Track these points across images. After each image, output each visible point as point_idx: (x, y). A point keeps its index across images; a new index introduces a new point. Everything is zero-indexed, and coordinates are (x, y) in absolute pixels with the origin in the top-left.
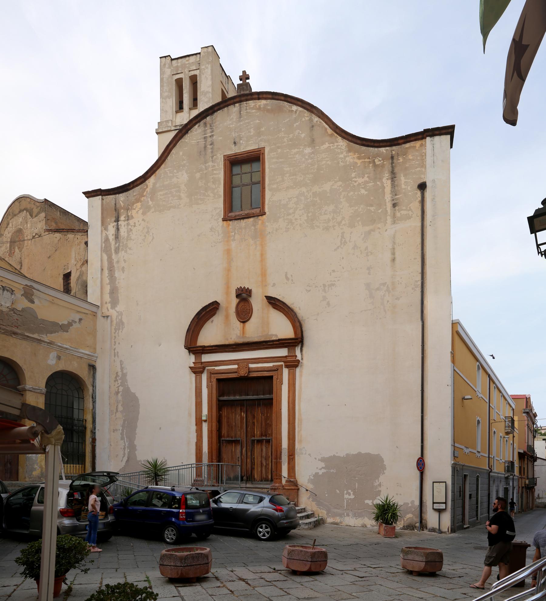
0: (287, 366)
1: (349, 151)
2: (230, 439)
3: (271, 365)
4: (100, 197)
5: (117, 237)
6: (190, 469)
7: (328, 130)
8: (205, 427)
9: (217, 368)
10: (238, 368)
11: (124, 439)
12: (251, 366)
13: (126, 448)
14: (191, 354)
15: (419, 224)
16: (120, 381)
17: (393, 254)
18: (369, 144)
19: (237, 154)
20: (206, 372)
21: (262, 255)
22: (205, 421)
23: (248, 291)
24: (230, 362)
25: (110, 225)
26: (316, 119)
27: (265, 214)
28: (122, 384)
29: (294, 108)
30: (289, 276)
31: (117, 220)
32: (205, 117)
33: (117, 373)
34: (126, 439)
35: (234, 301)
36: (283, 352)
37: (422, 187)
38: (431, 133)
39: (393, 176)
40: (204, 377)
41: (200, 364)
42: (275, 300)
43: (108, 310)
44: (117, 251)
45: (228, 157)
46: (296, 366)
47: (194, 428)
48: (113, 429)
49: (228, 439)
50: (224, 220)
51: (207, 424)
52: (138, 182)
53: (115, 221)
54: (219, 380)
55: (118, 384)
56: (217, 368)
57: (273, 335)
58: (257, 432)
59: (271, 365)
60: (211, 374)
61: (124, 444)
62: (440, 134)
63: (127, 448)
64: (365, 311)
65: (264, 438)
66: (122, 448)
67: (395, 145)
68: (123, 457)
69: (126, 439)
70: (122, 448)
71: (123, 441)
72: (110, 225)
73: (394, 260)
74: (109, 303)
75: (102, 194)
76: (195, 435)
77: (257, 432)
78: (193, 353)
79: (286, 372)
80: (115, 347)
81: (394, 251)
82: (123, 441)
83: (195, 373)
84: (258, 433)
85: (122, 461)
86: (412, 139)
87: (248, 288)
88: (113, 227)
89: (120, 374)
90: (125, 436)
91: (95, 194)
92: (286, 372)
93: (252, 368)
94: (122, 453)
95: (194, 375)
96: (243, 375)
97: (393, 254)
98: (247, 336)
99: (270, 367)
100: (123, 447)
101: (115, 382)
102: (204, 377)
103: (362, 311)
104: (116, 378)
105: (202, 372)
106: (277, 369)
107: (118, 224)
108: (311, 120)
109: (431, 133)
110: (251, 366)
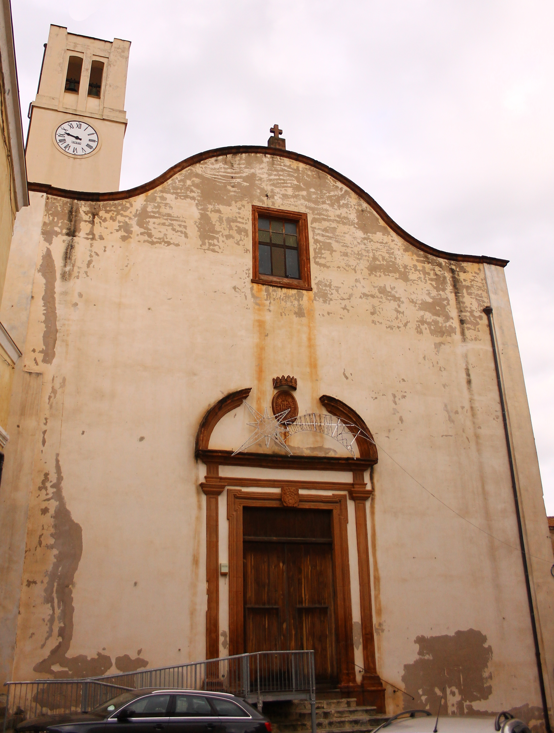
0: (352, 498)
1: (406, 250)
2: (261, 606)
3: (329, 493)
4: (45, 194)
5: (67, 256)
6: (194, 666)
7: (379, 220)
8: (224, 586)
9: (245, 490)
10: (281, 495)
11: (52, 601)
12: (302, 492)
13: (56, 619)
14: (199, 461)
15: (491, 349)
16: (51, 491)
17: (468, 375)
18: (428, 250)
19: (270, 209)
20: (225, 494)
21: (310, 339)
22: (224, 575)
23: (289, 380)
24: (269, 483)
25: (57, 236)
26: (365, 205)
27: (312, 290)
28: (58, 495)
29: (339, 184)
30: (348, 375)
31: (72, 233)
32: (226, 154)
33: (46, 475)
34: (56, 601)
35: (270, 392)
36: (346, 477)
37: (488, 311)
38: (488, 261)
39: (456, 291)
40: (222, 502)
41: (219, 480)
42: (338, 402)
43: (37, 363)
44: (65, 277)
45: (257, 208)
46: (366, 499)
47: (203, 586)
48: (28, 581)
49: (257, 606)
50: (253, 281)
51: (227, 580)
52: (106, 197)
53: (68, 234)
54: (245, 509)
55: (47, 494)
56: (245, 490)
57: (329, 449)
58: (305, 594)
59: (329, 493)
60: (234, 497)
61: (51, 612)
62: (496, 265)
63: (59, 620)
64: (446, 436)
65: (317, 606)
66: (46, 620)
67: (454, 260)
68: (47, 639)
69: (56, 601)
70: (46, 620)
71: (50, 604)
72: (57, 236)
73: (469, 382)
74: (40, 352)
75: (50, 191)
76: (204, 598)
77: (305, 594)
78: (205, 462)
79: (351, 506)
80: (44, 428)
81: (468, 371)
82: (50, 604)
83: (206, 493)
84: (307, 597)
85: (43, 646)
86: (470, 260)
87: (289, 377)
88: (64, 241)
89: (53, 478)
90: (55, 595)
91: (288, 155)
92: (351, 506)
93: (302, 495)
94: (47, 628)
95: (204, 498)
96: (290, 505)
97: (468, 375)
98: (292, 444)
99: (330, 496)
100: (49, 617)
101: (41, 490)
102: (222, 502)
103: (442, 436)
104: (43, 482)
105: (219, 493)
106: (340, 502)
107: (72, 240)
108: (360, 205)
109: (488, 261)
110: (302, 492)
